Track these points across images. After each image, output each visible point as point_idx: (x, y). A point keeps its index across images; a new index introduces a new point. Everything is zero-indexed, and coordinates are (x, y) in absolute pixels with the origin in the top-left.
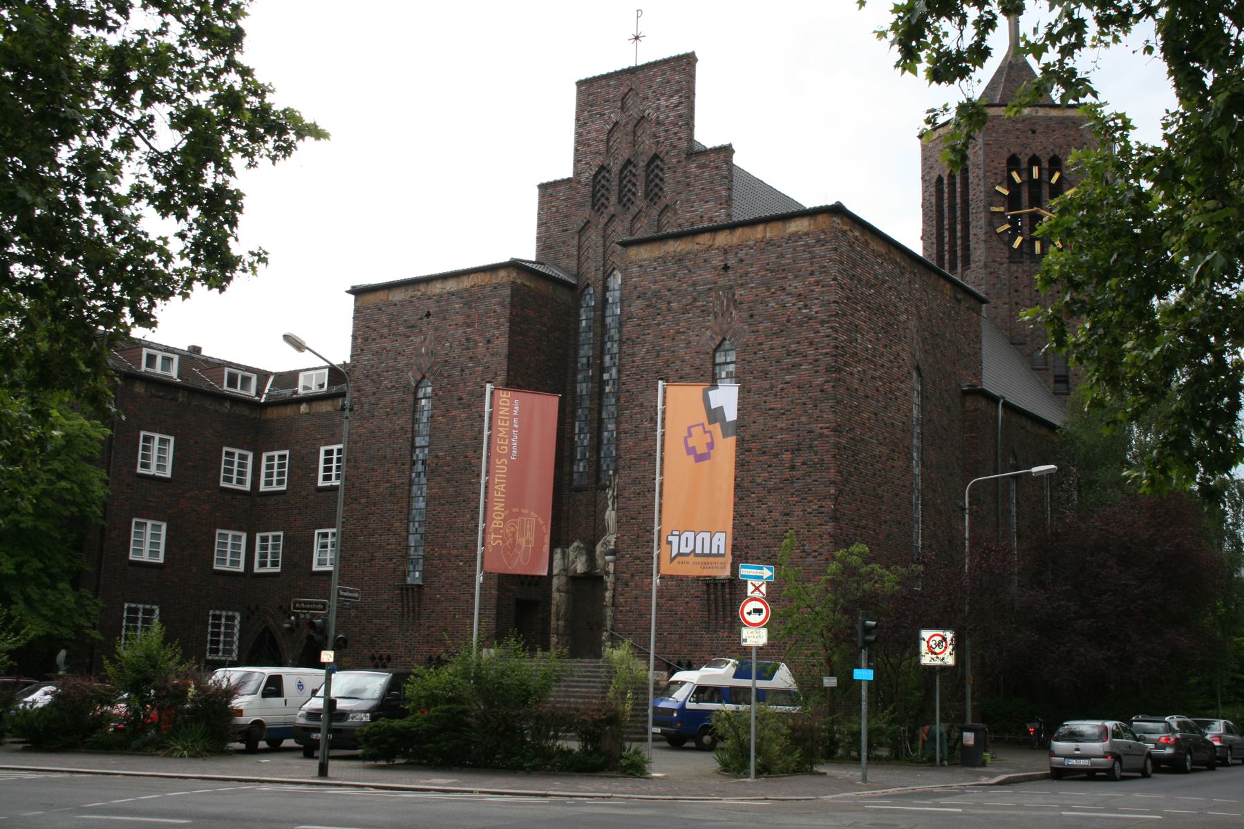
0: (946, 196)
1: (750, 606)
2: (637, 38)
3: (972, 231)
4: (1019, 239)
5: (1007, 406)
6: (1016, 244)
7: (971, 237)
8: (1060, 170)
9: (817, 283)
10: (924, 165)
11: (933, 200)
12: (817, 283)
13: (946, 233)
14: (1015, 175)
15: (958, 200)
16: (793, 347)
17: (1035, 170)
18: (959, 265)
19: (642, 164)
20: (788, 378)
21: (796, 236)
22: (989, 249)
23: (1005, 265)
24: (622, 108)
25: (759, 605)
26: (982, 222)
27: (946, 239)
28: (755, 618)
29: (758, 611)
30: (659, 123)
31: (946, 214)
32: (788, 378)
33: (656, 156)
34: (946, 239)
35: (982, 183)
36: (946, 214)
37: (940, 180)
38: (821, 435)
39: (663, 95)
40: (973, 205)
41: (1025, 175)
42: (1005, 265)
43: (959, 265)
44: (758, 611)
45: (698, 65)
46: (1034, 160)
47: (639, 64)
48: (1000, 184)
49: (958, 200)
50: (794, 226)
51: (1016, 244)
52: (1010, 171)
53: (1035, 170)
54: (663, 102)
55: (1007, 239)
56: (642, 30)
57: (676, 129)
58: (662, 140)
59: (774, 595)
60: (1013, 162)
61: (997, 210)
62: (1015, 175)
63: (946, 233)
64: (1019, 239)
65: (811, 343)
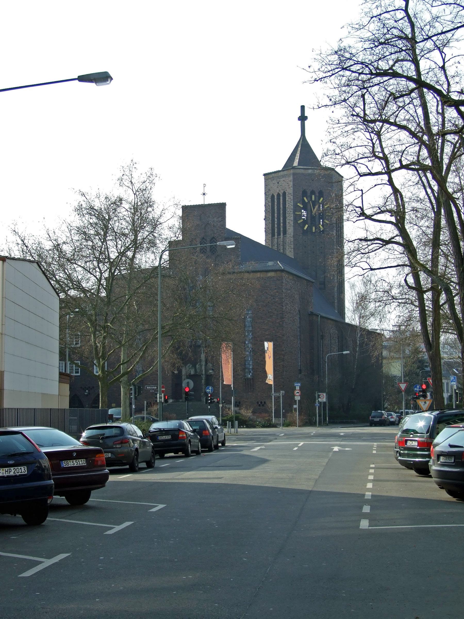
0: (276, 203)
1: (296, 392)
2: (204, 194)
3: (287, 221)
4: (307, 226)
5: (322, 317)
6: (305, 228)
7: (287, 224)
8: (323, 197)
9: (277, 292)
10: (265, 188)
11: (270, 204)
12: (277, 292)
13: (276, 220)
14: (305, 199)
15: (281, 206)
16: (270, 310)
17: (313, 197)
18: (282, 234)
19: (208, 240)
20: (269, 319)
21: (271, 277)
22: (295, 229)
23: (301, 237)
24: (200, 219)
25: (298, 391)
26: (292, 218)
27: (276, 222)
28: (297, 394)
29: (298, 393)
30: (214, 226)
31: (276, 212)
32: (269, 319)
33: (213, 238)
34: (276, 222)
35: (292, 201)
36: (276, 212)
37: (273, 196)
38: (279, 337)
39: (215, 217)
40: (288, 210)
41: (309, 198)
42: (301, 237)
43: (282, 234)
44: (298, 393)
45: (226, 207)
46: (313, 192)
47: (206, 203)
48: (299, 202)
49: (281, 206)
50: (270, 274)
51: (305, 228)
52: (303, 197)
53: (313, 197)
54: (215, 219)
55: (302, 225)
56: (206, 192)
57: (221, 230)
58: (216, 232)
59: (301, 389)
60: (304, 193)
61: (298, 213)
62: (305, 199)
63: (276, 220)
64: (307, 226)
65: (276, 310)
